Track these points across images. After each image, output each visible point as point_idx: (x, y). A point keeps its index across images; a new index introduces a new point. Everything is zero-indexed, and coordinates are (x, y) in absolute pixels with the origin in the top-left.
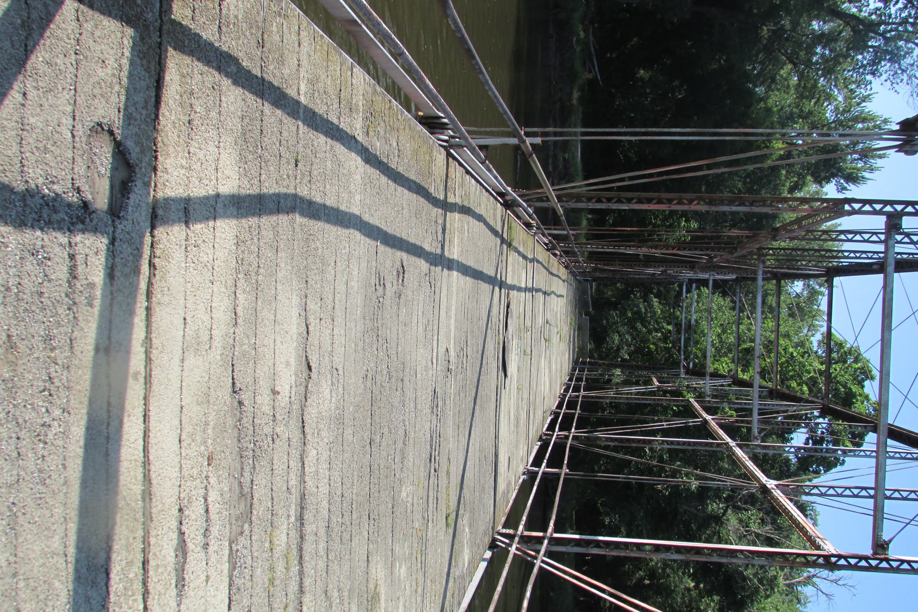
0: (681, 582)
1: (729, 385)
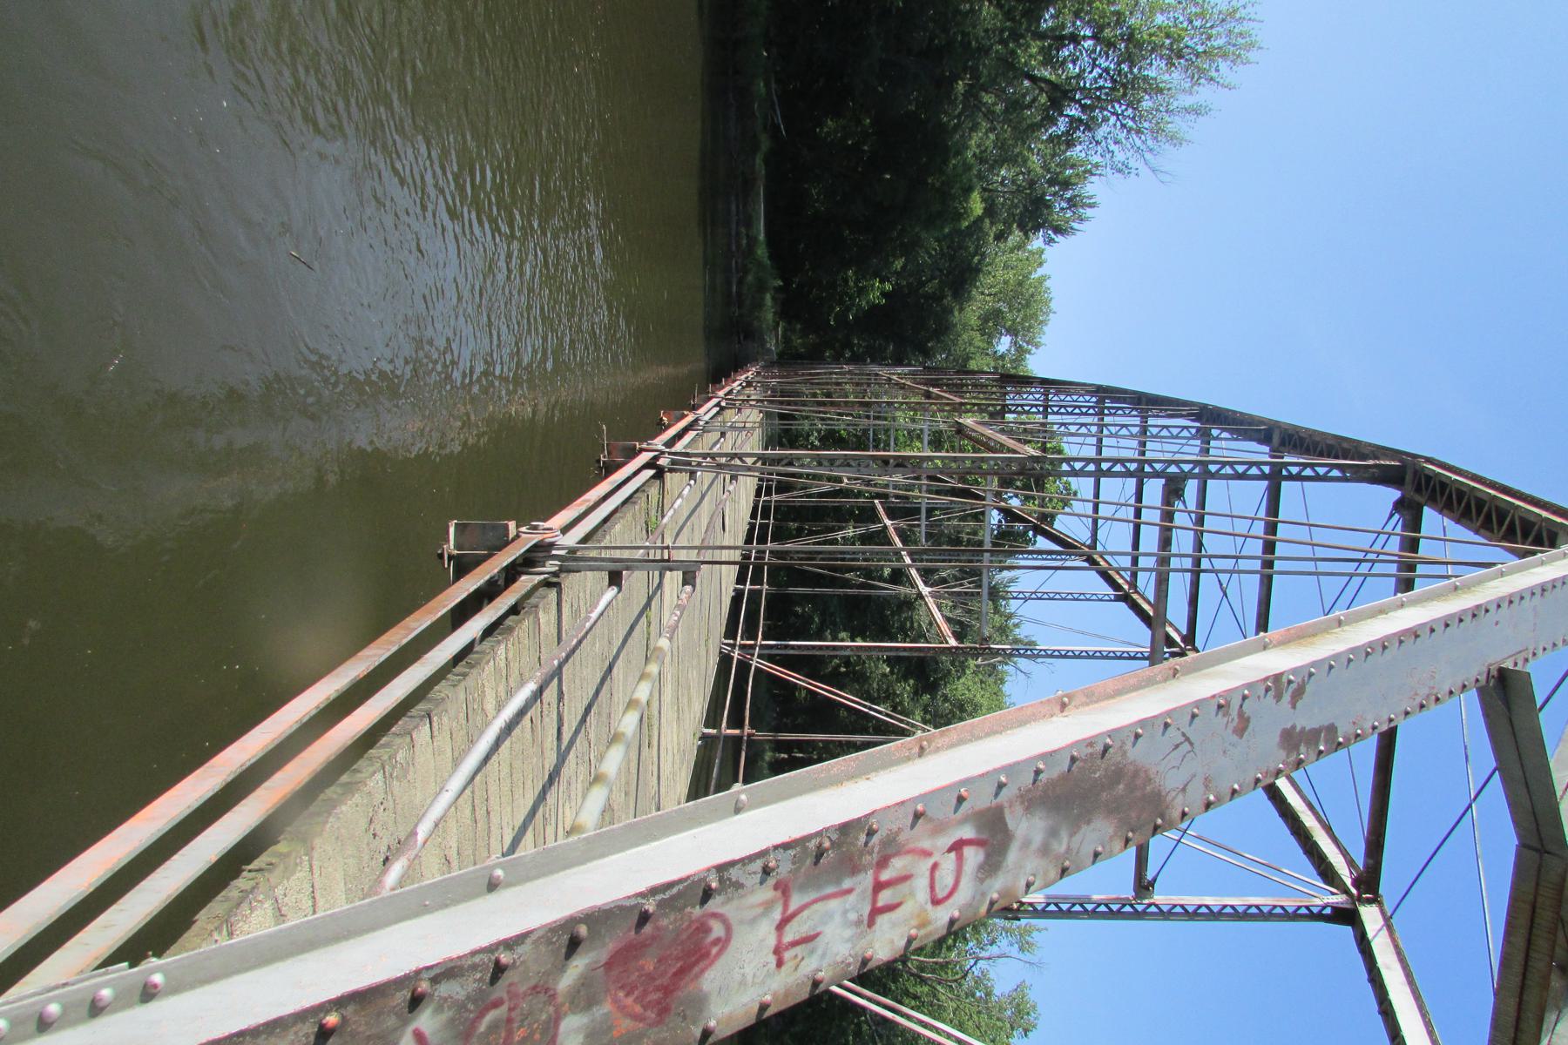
0: (877, 667)
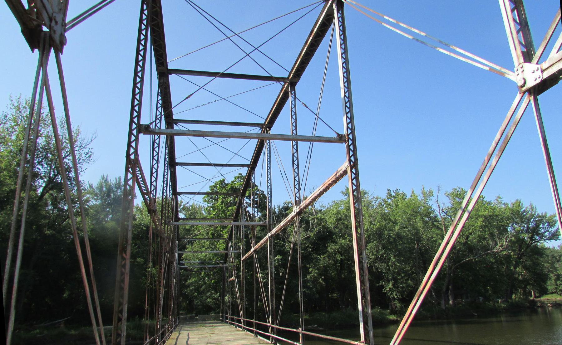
1: (232, 242)
